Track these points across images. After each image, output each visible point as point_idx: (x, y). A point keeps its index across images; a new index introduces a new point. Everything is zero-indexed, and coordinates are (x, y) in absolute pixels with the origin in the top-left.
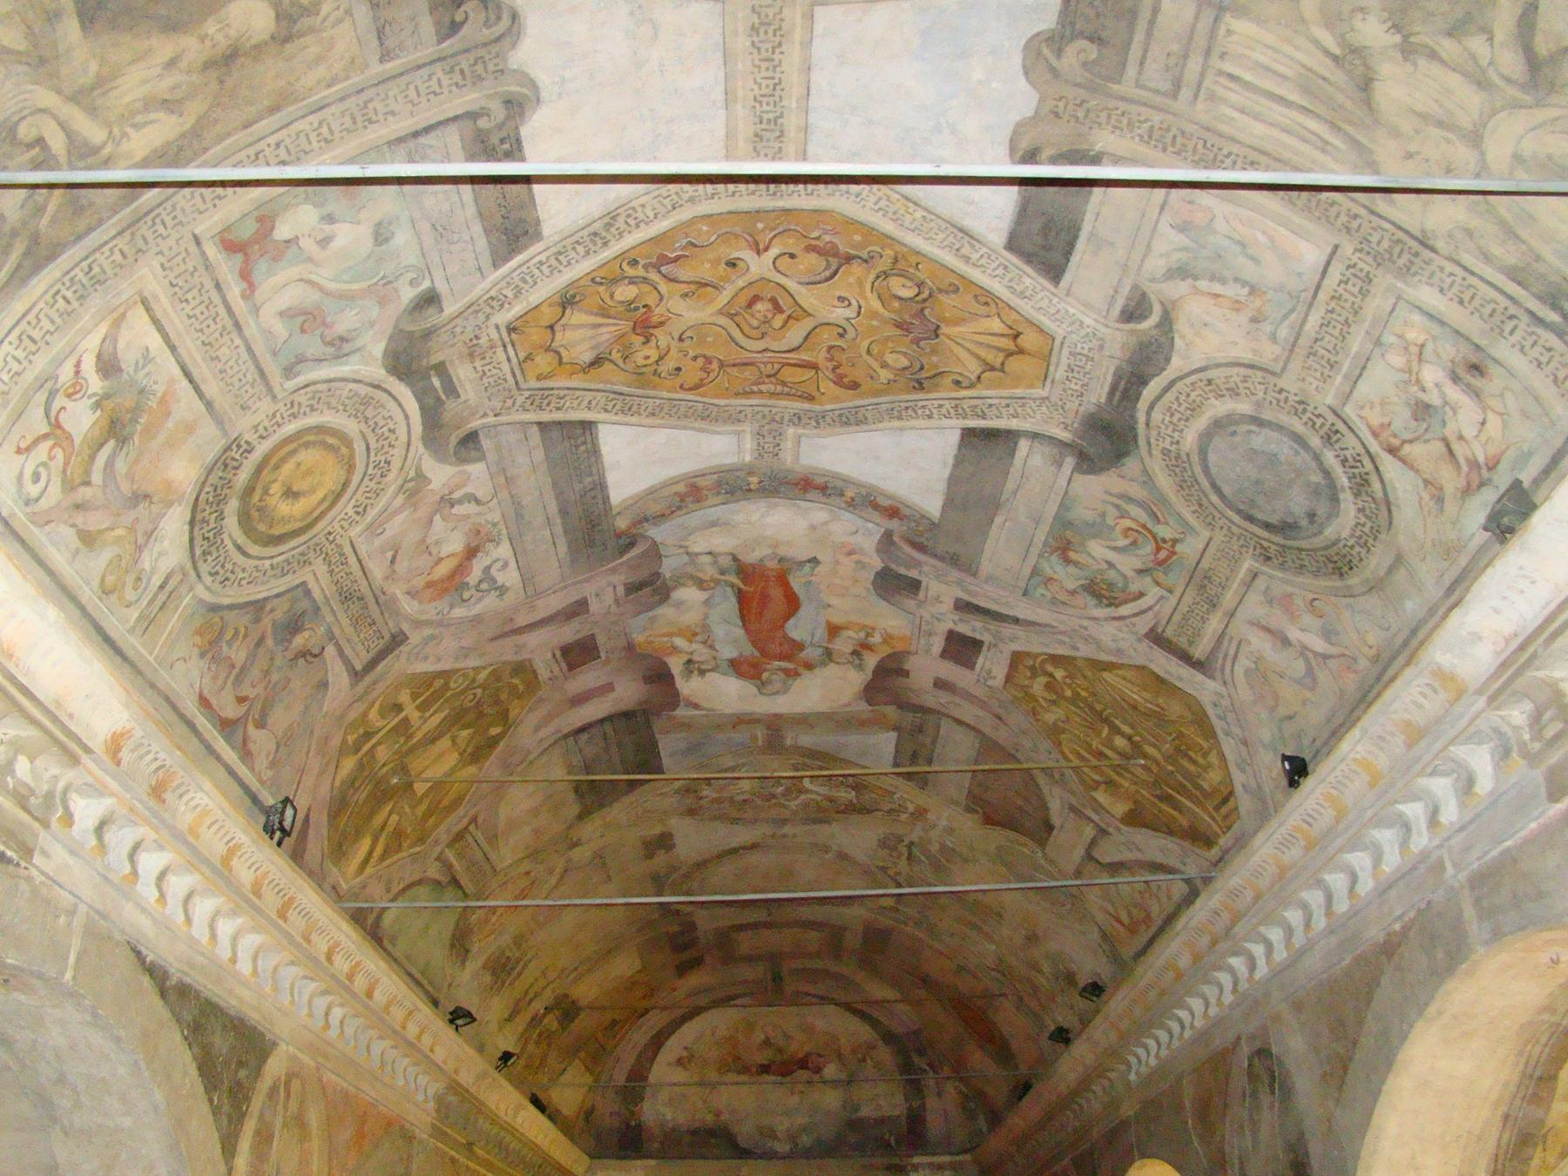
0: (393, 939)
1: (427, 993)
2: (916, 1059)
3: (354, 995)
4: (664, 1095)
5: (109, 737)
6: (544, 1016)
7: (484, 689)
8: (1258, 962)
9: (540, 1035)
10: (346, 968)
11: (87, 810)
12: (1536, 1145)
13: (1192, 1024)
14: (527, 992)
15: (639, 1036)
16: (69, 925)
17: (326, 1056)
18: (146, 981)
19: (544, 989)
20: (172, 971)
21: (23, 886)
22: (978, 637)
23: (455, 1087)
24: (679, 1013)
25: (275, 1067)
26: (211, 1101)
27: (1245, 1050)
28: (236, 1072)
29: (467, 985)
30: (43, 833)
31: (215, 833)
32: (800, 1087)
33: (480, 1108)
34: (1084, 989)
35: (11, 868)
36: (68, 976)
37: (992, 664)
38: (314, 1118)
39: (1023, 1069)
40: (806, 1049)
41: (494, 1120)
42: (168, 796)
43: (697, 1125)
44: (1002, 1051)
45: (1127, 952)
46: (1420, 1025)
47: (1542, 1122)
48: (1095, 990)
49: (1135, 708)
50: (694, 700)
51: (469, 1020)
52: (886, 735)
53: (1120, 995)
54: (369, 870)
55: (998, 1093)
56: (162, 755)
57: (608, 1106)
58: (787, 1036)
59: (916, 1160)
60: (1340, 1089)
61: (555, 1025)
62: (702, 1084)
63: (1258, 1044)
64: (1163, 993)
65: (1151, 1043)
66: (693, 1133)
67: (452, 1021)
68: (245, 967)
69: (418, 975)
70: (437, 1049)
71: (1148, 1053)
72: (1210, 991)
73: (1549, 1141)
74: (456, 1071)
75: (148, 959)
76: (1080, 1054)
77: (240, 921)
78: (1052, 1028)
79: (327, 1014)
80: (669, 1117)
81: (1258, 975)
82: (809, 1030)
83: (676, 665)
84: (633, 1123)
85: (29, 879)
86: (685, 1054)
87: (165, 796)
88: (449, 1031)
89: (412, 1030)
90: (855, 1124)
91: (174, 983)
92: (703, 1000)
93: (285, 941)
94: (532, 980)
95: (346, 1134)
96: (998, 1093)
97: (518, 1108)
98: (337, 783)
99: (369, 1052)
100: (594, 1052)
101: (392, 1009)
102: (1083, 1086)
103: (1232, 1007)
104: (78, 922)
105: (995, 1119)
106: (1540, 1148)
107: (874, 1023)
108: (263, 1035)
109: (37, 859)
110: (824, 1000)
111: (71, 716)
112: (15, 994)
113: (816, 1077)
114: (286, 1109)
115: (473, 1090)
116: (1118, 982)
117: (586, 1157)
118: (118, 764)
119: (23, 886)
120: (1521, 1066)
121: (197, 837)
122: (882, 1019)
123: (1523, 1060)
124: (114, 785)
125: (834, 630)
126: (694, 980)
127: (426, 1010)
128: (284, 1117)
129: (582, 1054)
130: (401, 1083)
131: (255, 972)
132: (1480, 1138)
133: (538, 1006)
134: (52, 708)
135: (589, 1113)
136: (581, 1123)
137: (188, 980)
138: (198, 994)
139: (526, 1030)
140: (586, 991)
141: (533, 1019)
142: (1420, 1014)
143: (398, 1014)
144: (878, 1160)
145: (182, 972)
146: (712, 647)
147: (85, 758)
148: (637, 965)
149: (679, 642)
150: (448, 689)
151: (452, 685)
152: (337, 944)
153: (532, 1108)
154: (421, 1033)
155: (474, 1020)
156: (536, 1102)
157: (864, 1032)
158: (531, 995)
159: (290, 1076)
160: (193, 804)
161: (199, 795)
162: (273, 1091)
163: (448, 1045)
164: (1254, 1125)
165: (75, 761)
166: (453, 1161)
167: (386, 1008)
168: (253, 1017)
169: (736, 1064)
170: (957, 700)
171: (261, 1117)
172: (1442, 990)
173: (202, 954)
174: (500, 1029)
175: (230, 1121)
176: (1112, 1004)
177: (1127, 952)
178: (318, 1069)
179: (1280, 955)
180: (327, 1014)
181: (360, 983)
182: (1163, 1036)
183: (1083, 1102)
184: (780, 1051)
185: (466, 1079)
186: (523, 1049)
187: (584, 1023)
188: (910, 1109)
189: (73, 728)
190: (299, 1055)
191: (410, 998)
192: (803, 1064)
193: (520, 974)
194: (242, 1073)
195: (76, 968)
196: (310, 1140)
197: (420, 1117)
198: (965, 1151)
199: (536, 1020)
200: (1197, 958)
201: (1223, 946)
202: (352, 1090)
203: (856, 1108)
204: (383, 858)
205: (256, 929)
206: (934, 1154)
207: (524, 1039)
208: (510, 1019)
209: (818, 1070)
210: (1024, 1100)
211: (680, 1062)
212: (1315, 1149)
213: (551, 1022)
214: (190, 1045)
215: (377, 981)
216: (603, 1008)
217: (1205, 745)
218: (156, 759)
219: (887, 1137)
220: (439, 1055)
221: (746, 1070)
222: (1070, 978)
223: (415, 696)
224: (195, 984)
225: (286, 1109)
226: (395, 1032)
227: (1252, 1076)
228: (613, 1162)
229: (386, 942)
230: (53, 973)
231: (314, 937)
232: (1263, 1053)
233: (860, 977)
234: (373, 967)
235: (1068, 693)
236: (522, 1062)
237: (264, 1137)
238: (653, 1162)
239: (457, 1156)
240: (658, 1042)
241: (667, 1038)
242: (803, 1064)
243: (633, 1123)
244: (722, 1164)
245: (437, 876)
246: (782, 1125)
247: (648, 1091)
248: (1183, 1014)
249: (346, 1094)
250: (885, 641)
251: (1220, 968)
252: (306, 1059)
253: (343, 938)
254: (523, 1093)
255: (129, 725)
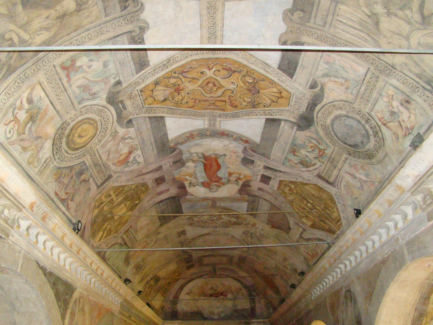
0: (109, 260)
1: (118, 274)
2: (253, 293)
3: (98, 275)
4: (183, 302)
5: (30, 204)
6: (150, 281)
7: (134, 191)
8: (347, 266)
9: (149, 286)
10: (96, 268)
11: (24, 224)
12: (424, 316)
13: (329, 283)
14: (145, 274)
15: (177, 286)
16: (19, 256)
17: (90, 292)
18: (40, 271)
19: (150, 273)
20: (47, 268)
21: (6, 245)
22: (270, 176)
23: (126, 300)
24: (187, 280)
25: (76, 295)
26: (58, 304)
27: (344, 290)
28: (65, 296)
29: (129, 272)
30: (12, 230)
31: (59, 230)
32: (221, 300)
33: (133, 306)
34: (299, 273)
35: (3, 240)
36: (19, 270)
37: (274, 184)
38: (87, 309)
39: (283, 296)
40: (223, 290)
41: (136, 309)
42: (46, 220)
43: (192, 311)
44: (277, 291)
45: (311, 263)
46: (392, 283)
47: (426, 310)
48: (302, 274)
49: (313, 196)
50: (192, 193)
51: (129, 282)
52: (245, 203)
53: (309, 275)
54: (102, 240)
55: (276, 302)
56: (45, 209)
57: (168, 306)
58: (217, 286)
59: (253, 321)
60: (370, 301)
61: (153, 283)
62: (194, 300)
63: (347, 289)
64: (321, 274)
65: (318, 288)
66: (191, 313)
67: (125, 282)
68: (68, 267)
69: (115, 270)
70: (121, 290)
71: (317, 291)
72: (334, 274)
73: (428, 315)
74: (126, 296)
75: (41, 265)
76: (298, 291)
77: (66, 254)
78: (291, 284)
79: (90, 280)
80: (185, 309)
81: (347, 270)
82: (223, 285)
83: (187, 184)
84: (175, 310)
85: (8, 243)
86: (189, 291)
87: (45, 220)
88: (124, 285)
89: (114, 285)
90: (236, 311)
91: (48, 272)
92: (194, 276)
93: (79, 260)
94: (147, 271)
95: (95, 313)
96: (276, 302)
97: (143, 306)
98: (93, 216)
99: (102, 291)
100: (164, 291)
101: (108, 279)
102: (299, 300)
103: (340, 278)
104: (21, 255)
105: (275, 309)
106: (425, 317)
107: (241, 283)
108: (73, 286)
109: (10, 237)
110: (227, 276)
111: (20, 198)
112: (4, 275)
113: (225, 298)
114: (79, 307)
115: (131, 301)
116: (309, 271)
117: (162, 320)
118: (33, 211)
119: (6, 245)
120: (420, 295)
121: (54, 231)
122: (244, 282)
123: (421, 293)
124: (31, 217)
125: (230, 174)
126: (192, 271)
127: (118, 279)
128: (78, 309)
129: (161, 291)
130: (111, 299)
131: (70, 269)
132: (409, 315)
133: (149, 278)
134: (14, 196)
135: (163, 308)
136: (160, 310)
137: (52, 271)
138: (55, 275)
139: (145, 285)
140: (162, 274)
141: (147, 282)
142: (392, 280)
143: (110, 280)
144: (243, 321)
145: (50, 268)
146: (197, 179)
147: (23, 210)
148: (176, 267)
149: (188, 177)
150: (124, 190)
151: (125, 189)
152: (93, 261)
153: (147, 306)
154: (116, 285)
155: (131, 282)
156: (148, 305)
157: (239, 285)
158: (147, 275)
159: (80, 297)
160: (53, 222)
161: (55, 220)
162: (75, 302)
163: (124, 289)
164: (346, 311)
165: (21, 210)
166: (125, 321)
167: (107, 279)
168: (70, 281)
169: (203, 294)
170: (264, 193)
171: (72, 309)
172: (398, 273)
173: (56, 264)
174: (138, 284)
175: (64, 310)
176: (307, 277)
177: (311, 263)
178: (88, 295)
179: (354, 264)
180: (90, 280)
181: (99, 272)
182: (321, 286)
183: (299, 305)
184: (215, 290)
185: (129, 298)
186: (145, 290)
187: (161, 283)
188: (251, 306)
189: (20, 201)
190: (83, 291)
191: (113, 276)
192: (222, 294)
193: (143, 269)
194: (67, 297)
195: (21, 268)
196: (86, 315)
197: (116, 309)
198: (267, 318)
199: (148, 282)
200: (331, 265)
201: (338, 261)
202: (97, 301)
203: (236, 306)
204: (106, 237)
205: (71, 257)
206: (258, 319)
207: (145, 287)
208: (141, 282)
209: (226, 296)
210: (283, 304)
211: (188, 293)
212: (363, 318)
213: (152, 282)
214: (52, 289)
215: (104, 271)
216: (167, 279)
217: (333, 206)
218: (43, 210)
219: (245, 314)
220: (121, 291)
221: (206, 296)
222: (296, 270)
223: (114, 192)
224: (54, 272)
225: (79, 307)
226: (109, 285)
227: (346, 297)
228: (169, 321)
229: (107, 260)
230: (14, 269)
231: (87, 259)
232: (349, 291)
233: (237, 270)
234: (103, 267)
235: (295, 192)
236: (144, 294)
237: (73, 314)
238: (180, 321)
239: (126, 320)
240: (182, 288)
241: (184, 287)
242: (222, 294)
243: (175, 310)
244: (199, 322)
245: (121, 242)
246: (216, 311)
247: (179, 302)
248: (327, 280)
249: (96, 302)
250: (244, 177)
251: (337, 268)
252: (85, 293)
253: (95, 259)
254: (144, 302)
255: (35, 200)
